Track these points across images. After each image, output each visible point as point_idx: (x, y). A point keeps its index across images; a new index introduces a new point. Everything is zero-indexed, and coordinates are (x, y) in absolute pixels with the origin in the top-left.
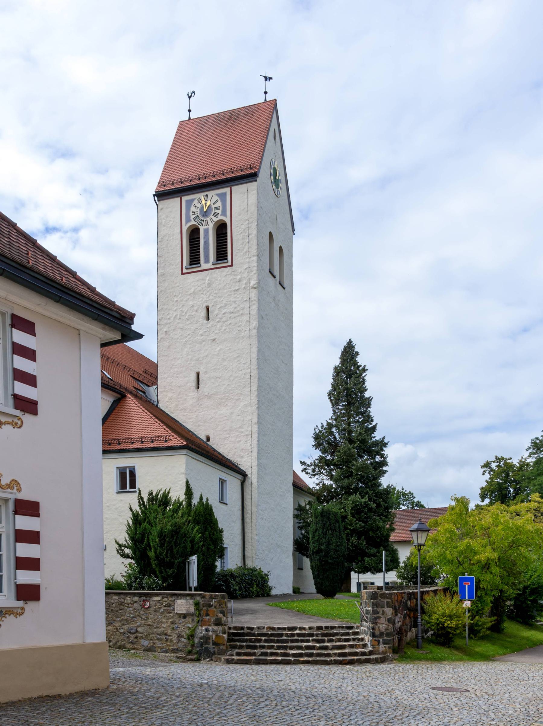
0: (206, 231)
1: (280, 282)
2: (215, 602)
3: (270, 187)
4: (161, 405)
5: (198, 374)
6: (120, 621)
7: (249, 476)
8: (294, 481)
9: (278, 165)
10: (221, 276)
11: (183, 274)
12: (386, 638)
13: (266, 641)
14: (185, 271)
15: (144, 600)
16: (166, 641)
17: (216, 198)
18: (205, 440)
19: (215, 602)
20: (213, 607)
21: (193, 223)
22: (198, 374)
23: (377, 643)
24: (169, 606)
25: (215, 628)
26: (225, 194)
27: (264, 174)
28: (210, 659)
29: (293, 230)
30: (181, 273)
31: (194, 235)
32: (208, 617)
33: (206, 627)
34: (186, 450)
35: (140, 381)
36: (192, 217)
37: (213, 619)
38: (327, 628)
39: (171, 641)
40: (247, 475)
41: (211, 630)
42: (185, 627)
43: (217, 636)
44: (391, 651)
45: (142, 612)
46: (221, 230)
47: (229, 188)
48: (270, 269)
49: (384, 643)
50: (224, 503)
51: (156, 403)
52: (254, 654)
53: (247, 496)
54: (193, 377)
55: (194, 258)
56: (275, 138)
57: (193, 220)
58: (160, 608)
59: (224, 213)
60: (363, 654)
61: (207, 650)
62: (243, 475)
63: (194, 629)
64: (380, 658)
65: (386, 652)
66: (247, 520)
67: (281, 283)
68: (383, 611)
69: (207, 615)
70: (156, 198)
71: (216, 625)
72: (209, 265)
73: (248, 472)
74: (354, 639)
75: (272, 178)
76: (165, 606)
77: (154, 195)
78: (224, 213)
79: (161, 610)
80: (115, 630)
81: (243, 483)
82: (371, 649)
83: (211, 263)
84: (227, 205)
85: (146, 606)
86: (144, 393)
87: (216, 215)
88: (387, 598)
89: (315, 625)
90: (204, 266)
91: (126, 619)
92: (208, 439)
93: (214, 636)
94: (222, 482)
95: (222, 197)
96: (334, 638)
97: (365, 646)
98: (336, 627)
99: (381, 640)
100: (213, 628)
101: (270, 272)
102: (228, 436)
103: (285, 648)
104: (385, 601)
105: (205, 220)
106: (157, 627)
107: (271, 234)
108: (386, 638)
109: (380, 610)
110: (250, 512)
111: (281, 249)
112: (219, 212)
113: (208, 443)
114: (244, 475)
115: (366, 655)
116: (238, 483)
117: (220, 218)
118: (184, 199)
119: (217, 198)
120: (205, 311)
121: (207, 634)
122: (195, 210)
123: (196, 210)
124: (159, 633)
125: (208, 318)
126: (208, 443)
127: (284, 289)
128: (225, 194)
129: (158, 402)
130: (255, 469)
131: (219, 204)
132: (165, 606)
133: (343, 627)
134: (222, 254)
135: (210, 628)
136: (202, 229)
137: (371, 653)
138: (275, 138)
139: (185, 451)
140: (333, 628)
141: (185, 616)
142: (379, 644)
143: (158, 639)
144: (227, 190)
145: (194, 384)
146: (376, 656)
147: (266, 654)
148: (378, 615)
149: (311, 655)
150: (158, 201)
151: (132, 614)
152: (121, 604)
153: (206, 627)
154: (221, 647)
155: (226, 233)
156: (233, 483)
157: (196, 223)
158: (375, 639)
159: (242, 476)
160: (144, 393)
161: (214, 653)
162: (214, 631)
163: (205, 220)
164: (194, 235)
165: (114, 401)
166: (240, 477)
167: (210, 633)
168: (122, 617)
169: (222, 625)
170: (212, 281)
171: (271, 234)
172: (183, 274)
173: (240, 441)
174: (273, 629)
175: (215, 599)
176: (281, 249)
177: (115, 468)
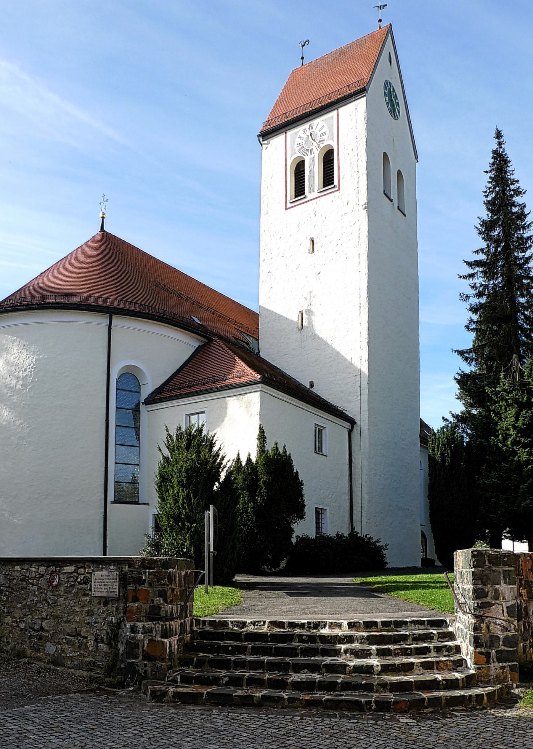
1: (398, 207)
2: (150, 574)
3: (382, 101)
4: (262, 355)
6: (21, 609)
7: (358, 423)
11: (286, 209)
13: (255, 651)
14: (289, 205)
15: (53, 572)
16: (80, 647)
20: (146, 585)
21: (299, 155)
23: (483, 658)
24: (86, 583)
27: (376, 89)
28: (137, 686)
29: (416, 157)
30: (284, 208)
33: (132, 623)
36: (297, 149)
37: (146, 607)
38: (386, 624)
39: (87, 647)
41: (141, 630)
42: (104, 619)
44: (517, 676)
45: (49, 594)
46: (328, 160)
47: (335, 112)
48: (384, 191)
49: (499, 660)
50: (323, 455)
51: (257, 351)
52: (216, 681)
55: (300, 190)
56: (390, 62)
57: (297, 152)
58: (73, 586)
60: (452, 684)
61: (132, 669)
63: (119, 625)
64: (488, 694)
65: (506, 677)
66: (356, 476)
67: (400, 208)
68: (497, 591)
69: (136, 599)
70: (261, 139)
71: (150, 619)
72: (315, 194)
74: (438, 650)
75: (387, 98)
76: (80, 583)
77: (259, 136)
79: (75, 590)
80: (15, 624)
81: (350, 432)
82: (472, 671)
83: (316, 192)
85: (55, 583)
86: (248, 344)
88: (505, 564)
89: (360, 618)
91: (29, 606)
92: (312, 385)
93: (146, 641)
94: (319, 431)
96: (391, 647)
97: (460, 664)
98: (406, 623)
100: (144, 626)
101: (385, 194)
102: (334, 379)
103: (284, 668)
104: (501, 569)
105: (310, 149)
106: (67, 622)
107: (385, 155)
108: (503, 648)
109: (489, 588)
111: (399, 173)
112: (325, 137)
113: (312, 389)
114: (352, 422)
115: (457, 688)
117: (326, 143)
120: (309, 243)
121: (134, 638)
122: (300, 141)
123: (302, 141)
124: (69, 631)
126: (312, 389)
127: (405, 216)
129: (259, 350)
130: (365, 415)
132: (80, 583)
133: (422, 623)
134: (328, 179)
135: (140, 625)
137: (470, 681)
138: (390, 62)
140: (399, 624)
141: (106, 601)
142: (488, 662)
143: (68, 642)
146: (479, 691)
147: (236, 682)
148: (485, 600)
149: (330, 686)
151: (36, 596)
152: (24, 579)
153: (132, 623)
154: (158, 664)
155: (333, 159)
156: (335, 431)
157: (300, 155)
158: (479, 650)
159: (349, 424)
160: (248, 344)
161: (145, 676)
162: (147, 631)
163: (310, 149)
165: (199, 346)
166: (348, 425)
167: (140, 636)
168: (24, 602)
169: (161, 619)
171: (385, 155)
172: (286, 209)
173: (347, 384)
174: (280, 625)
175: (150, 568)
176: (399, 173)
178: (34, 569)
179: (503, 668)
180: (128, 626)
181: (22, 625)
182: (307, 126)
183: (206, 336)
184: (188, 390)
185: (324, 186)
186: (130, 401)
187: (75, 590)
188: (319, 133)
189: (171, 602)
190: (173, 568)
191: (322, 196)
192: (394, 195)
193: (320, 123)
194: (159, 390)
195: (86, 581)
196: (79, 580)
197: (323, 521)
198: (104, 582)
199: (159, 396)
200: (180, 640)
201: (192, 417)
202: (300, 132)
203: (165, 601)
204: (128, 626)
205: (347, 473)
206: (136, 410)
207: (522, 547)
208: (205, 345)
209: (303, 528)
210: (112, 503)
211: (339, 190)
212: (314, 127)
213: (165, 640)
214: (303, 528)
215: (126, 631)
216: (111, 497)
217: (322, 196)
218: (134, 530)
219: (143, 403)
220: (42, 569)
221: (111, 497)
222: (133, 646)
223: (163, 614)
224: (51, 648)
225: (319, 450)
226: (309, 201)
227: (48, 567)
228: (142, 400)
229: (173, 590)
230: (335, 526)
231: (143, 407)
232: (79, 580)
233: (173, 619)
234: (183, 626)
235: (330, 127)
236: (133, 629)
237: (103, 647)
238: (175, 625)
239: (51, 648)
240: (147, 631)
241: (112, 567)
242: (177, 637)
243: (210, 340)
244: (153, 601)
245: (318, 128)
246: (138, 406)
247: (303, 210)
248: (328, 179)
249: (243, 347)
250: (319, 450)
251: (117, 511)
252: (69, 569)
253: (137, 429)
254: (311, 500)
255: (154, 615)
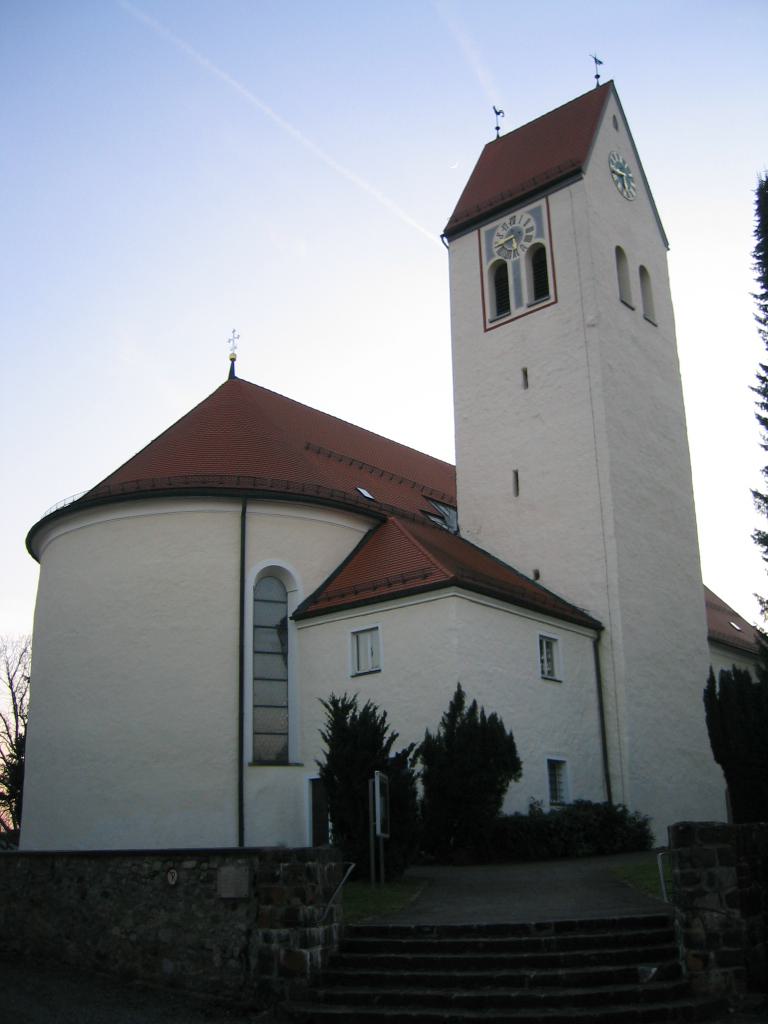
0: (517, 265)
2: (284, 869)
4: (464, 534)
5: (516, 474)
7: (608, 628)
8: (709, 631)
9: (625, 156)
10: (544, 321)
11: (486, 330)
12: (725, 948)
14: (489, 326)
17: (527, 216)
18: (531, 576)
19: (284, 869)
21: (497, 257)
22: (516, 474)
25: (284, 931)
26: (539, 208)
31: (500, 274)
32: (270, 907)
34: (454, 588)
35: (433, 500)
36: (495, 251)
40: (603, 629)
43: (289, 952)
46: (538, 258)
47: (544, 200)
49: (721, 963)
53: (605, 665)
54: (511, 478)
55: (502, 305)
59: (540, 234)
62: (592, 628)
69: (269, 901)
70: (445, 240)
71: (287, 925)
72: (523, 310)
73: (605, 622)
76: (202, 881)
77: (442, 236)
78: (540, 234)
79: (197, 891)
80: (124, 936)
83: (525, 306)
84: (543, 222)
87: (528, 239)
90: (515, 311)
92: (537, 575)
93: (282, 952)
94: (547, 644)
95: (536, 213)
99: (712, 955)
101: (622, 302)
107: (619, 251)
108: (725, 948)
110: (613, 694)
111: (643, 270)
112: (533, 233)
114: (597, 627)
116: (589, 644)
117: (535, 241)
118: (483, 230)
119: (529, 216)
120: (520, 376)
125: (526, 385)
126: (538, 582)
128: (539, 208)
131: (532, 223)
134: (541, 289)
135: (274, 932)
136: (510, 263)
139: (452, 591)
141: (233, 903)
144: (542, 202)
145: (511, 489)
150: (449, 241)
156: (571, 645)
157: (500, 258)
158: (693, 952)
159: (592, 631)
160: (442, 518)
164: (500, 274)
166: (591, 633)
167: (275, 946)
170: (534, 330)
172: (486, 330)
176: (643, 270)
177: (350, 635)
178: (146, 866)
179: (725, 974)
180: (260, 934)
181: (133, 937)
182: (506, 219)
183: (375, 517)
184: (353, 598)
185: (536, 299)
186: (275, 619)
187: (197, 891)
188: (524, 229)
189: (311, 903)
190: (313, 860)
191: (531, 312)
192: (636, 299)
193: (522, 216)
194: (313, 599)
195: (211, 879)
196: (202, 878)
197: (562, 779)
198: (232, 880)
199: (313, 608)
200: (324, 953)
201: (361, 636)
202: (501, 226)
203: (304, 901)
204: (260, 934)
205: (596, 704)
206: (282, 629)
207: (452, 839)
208: (378, 526)
209: (522, 796)
210: (250, 765)
211: (556, 302)
212: (517, 221)
213: (304, 951)
214: (522, 796)
215: (258, 940)
216: (248, 756)
217: (531, 312)
218: (284, 809)
219: (291, 618)
220: (158, 865)
221: (248, 756)
222: (266, 958)
223: (301, 919)
224: (168, 966)
225: (549, 676)
226: (516, 318)
227: (164, 862)
228: (290, 615)
229: (314, 888)
230: (581, 787)
231: (291, 624)
232: (202, 878)
233: (315, 925)
234: (328, 934)
235: (539, 220)
236: (267, 938)
237: (233, 963)
238: (318, 931)
239: (168, 966)
240: (284, 941)
241: (240, 861)
242: (320, 948)
243: (383, 521)
244: (289, 902)
245: (523, 222)
246: (284, 622)
247: (507, 333)
248: (541, 289)
249: (435, 526)
250: (549, 676)
251: (260, 778)
252: (189, 864)
253: (285, 655)
254: (532, 753)
255: (291, 920)
